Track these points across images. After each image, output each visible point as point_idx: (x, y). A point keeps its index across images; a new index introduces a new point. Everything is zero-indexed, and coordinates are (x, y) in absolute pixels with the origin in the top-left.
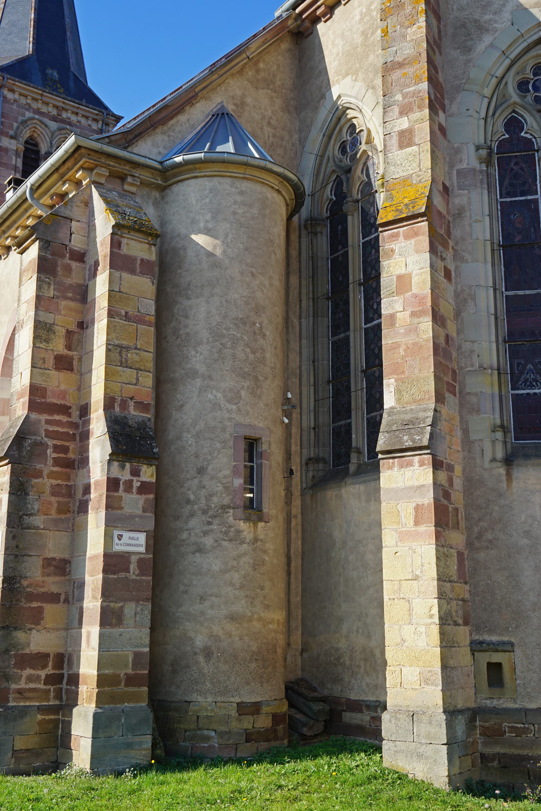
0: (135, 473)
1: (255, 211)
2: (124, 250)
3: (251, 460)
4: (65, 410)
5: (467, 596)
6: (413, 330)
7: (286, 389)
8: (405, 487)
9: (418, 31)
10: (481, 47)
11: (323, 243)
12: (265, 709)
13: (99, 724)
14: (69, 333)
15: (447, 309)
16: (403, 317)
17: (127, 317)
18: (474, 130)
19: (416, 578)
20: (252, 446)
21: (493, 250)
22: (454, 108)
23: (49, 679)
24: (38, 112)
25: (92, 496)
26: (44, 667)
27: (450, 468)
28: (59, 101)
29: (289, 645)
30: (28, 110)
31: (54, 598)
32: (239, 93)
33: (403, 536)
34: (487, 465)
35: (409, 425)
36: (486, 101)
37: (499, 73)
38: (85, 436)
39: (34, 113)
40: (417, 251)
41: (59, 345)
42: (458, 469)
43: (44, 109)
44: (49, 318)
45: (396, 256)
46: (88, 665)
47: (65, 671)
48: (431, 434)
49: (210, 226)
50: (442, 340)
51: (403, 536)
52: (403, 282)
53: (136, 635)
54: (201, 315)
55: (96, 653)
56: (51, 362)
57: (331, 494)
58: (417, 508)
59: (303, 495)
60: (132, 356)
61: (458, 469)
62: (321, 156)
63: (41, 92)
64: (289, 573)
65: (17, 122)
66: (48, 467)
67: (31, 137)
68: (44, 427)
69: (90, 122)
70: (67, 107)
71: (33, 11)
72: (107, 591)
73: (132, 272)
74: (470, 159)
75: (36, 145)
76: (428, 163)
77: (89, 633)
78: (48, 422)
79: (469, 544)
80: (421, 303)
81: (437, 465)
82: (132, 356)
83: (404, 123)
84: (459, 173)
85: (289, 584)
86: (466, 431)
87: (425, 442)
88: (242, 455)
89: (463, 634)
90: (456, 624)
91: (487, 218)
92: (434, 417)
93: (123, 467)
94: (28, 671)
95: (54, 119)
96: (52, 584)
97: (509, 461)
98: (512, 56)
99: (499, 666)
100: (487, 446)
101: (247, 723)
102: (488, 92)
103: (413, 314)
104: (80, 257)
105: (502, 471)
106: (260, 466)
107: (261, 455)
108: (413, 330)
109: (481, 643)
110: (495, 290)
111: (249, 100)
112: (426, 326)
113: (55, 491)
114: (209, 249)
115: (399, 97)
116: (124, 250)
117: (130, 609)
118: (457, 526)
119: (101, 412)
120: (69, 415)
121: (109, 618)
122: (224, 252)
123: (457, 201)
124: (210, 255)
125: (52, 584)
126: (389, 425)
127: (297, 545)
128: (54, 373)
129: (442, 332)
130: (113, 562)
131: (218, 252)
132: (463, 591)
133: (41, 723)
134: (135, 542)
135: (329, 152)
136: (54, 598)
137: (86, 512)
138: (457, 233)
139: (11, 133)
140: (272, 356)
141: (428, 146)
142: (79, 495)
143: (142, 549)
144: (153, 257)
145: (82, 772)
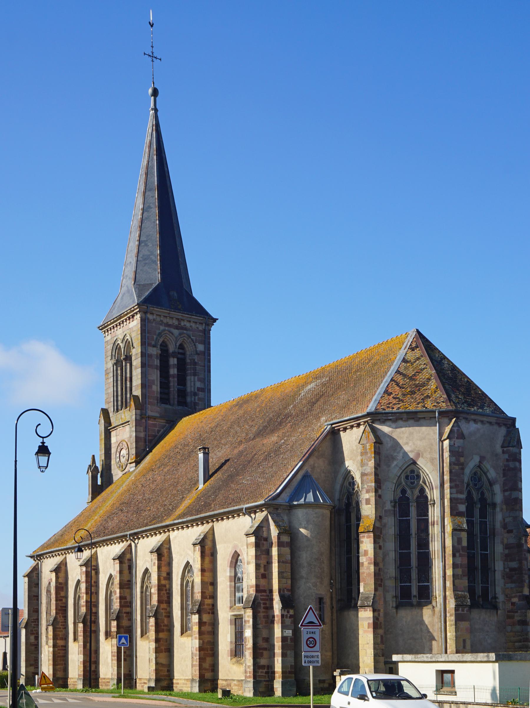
0: (288, 612)
1: (320, 519)
2: (281, 540)
3: (320, 604)
4: (264, 591)
5: (384, 648)
6: (368, 568)
7: (331, 579)
8: (365, 616)
9: (371, 464)
10: (393, 465)
11: (343, 519)
12: (326, 682)
13: (283, 684)
14: (265, 566)
15: (379, 559)
16: (366, 564)
17: (283, 562)
18: (389, 495)
19: (368, 644)
20: (321, 600)
21: (395, 538)
22: (384, 487)
23: (266, 673)
24: (167, 325)
25: (276, 619)
26: (265, 669)
27: (379, 610)
28: (179, 315)
29: (333, 663)
30: (161, 324)
31: (265, 649)
32: (312, 463)
33: (365, 632)
34: (391, 608)
35: (367, 598)
36: (394, 485)
37: (399, 475)
38: (272, 600)
39: (165, 326)
40: (370, 543)
41: (262, 571)
42: (382, 610)
43: (170, 322)
44: (259, 562)
45: (364, 543)
46: (278, 667)
47: (270, 670)
48: (373, 602)
49: (306, 526)
50: (377, 571)
51: (365, 632)
52: (366, 552)
53: (291, 660)
54: (304, 557)
55: (281, 665)
56: (260, 576)
57: (346, 613)
58: (369, 624)
59: (337, 612)
60: (285, 575)
61: (382, 610)
62: (342, 485)
63: (168, 312)
64: (332, 639)
65: (155, 335)
66: (262, 610)
67: (163, 342)
68: (260, 597)
69: (197, 326)
70: (184, 318)
71: (158, 248)
72: (283, 647)
73: (284, 547)
74: (388, 506)
75: (166, 346)
76: (374, 512)
77: (278, 660)
78: (261, 596)
79: (385, 633)
80: (371, 560)
81: (374, 611)
82: (285, 575)
83: (367, 496)
84: (385, 511)
85: (332, 643)
86: (385, 598)
87: (371, 605)
88: (318, 603)
89: (382, 659)
90: (379, 656)
91: (393, 527)
92: (374, 597)
93: (285, 611)
94: (261, 670)
95: (177, 328)
96: (265, 645)
97: (397, 607)
98: (403, 469)
99: (392, 668)
100: (391, 603)
101: (321, 685)
102: (395, 481)
103: (369, 563)
104: (266, 539)
105: (395, 611)
106: (323, 607)
107: (324, 603)
108: (368, 568)
109: (387, 661)
110: (395, 551)
111: (316, 465)
112: (372, 567)
113: (264, 617)
114: (306, 534)
115: (366, 486)
116: (281, 540)
117: (289, 652)
118: (381, 628)
119: (277, 593)
120: (266, 592)
121: (284, 655)
122: (311, 536)
123: (384, 521)
124: (306, 536)
125: (265, 645)
126: (361, 598)
127: (335, 630)
128: (261, 580)
129: (377, 568)
130: (284, 639)
131: (309, 536)
132: (383, 646)
133: (265, 684)
134: (289, 633)
135: (345, 484)
136: (265, 649)
137: (274, 623)
138: (384, 532)
139: (153, 343)
140: (326, 569)
141: (374, 506)
142: (271, 618)
143: (291, 635)
144: (289, 540)
145: (279, 697)
